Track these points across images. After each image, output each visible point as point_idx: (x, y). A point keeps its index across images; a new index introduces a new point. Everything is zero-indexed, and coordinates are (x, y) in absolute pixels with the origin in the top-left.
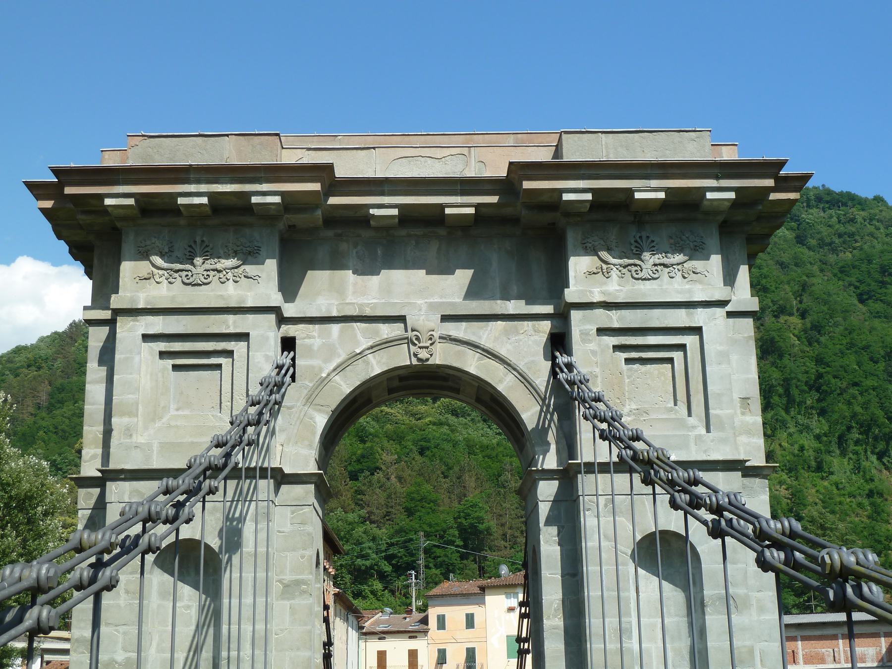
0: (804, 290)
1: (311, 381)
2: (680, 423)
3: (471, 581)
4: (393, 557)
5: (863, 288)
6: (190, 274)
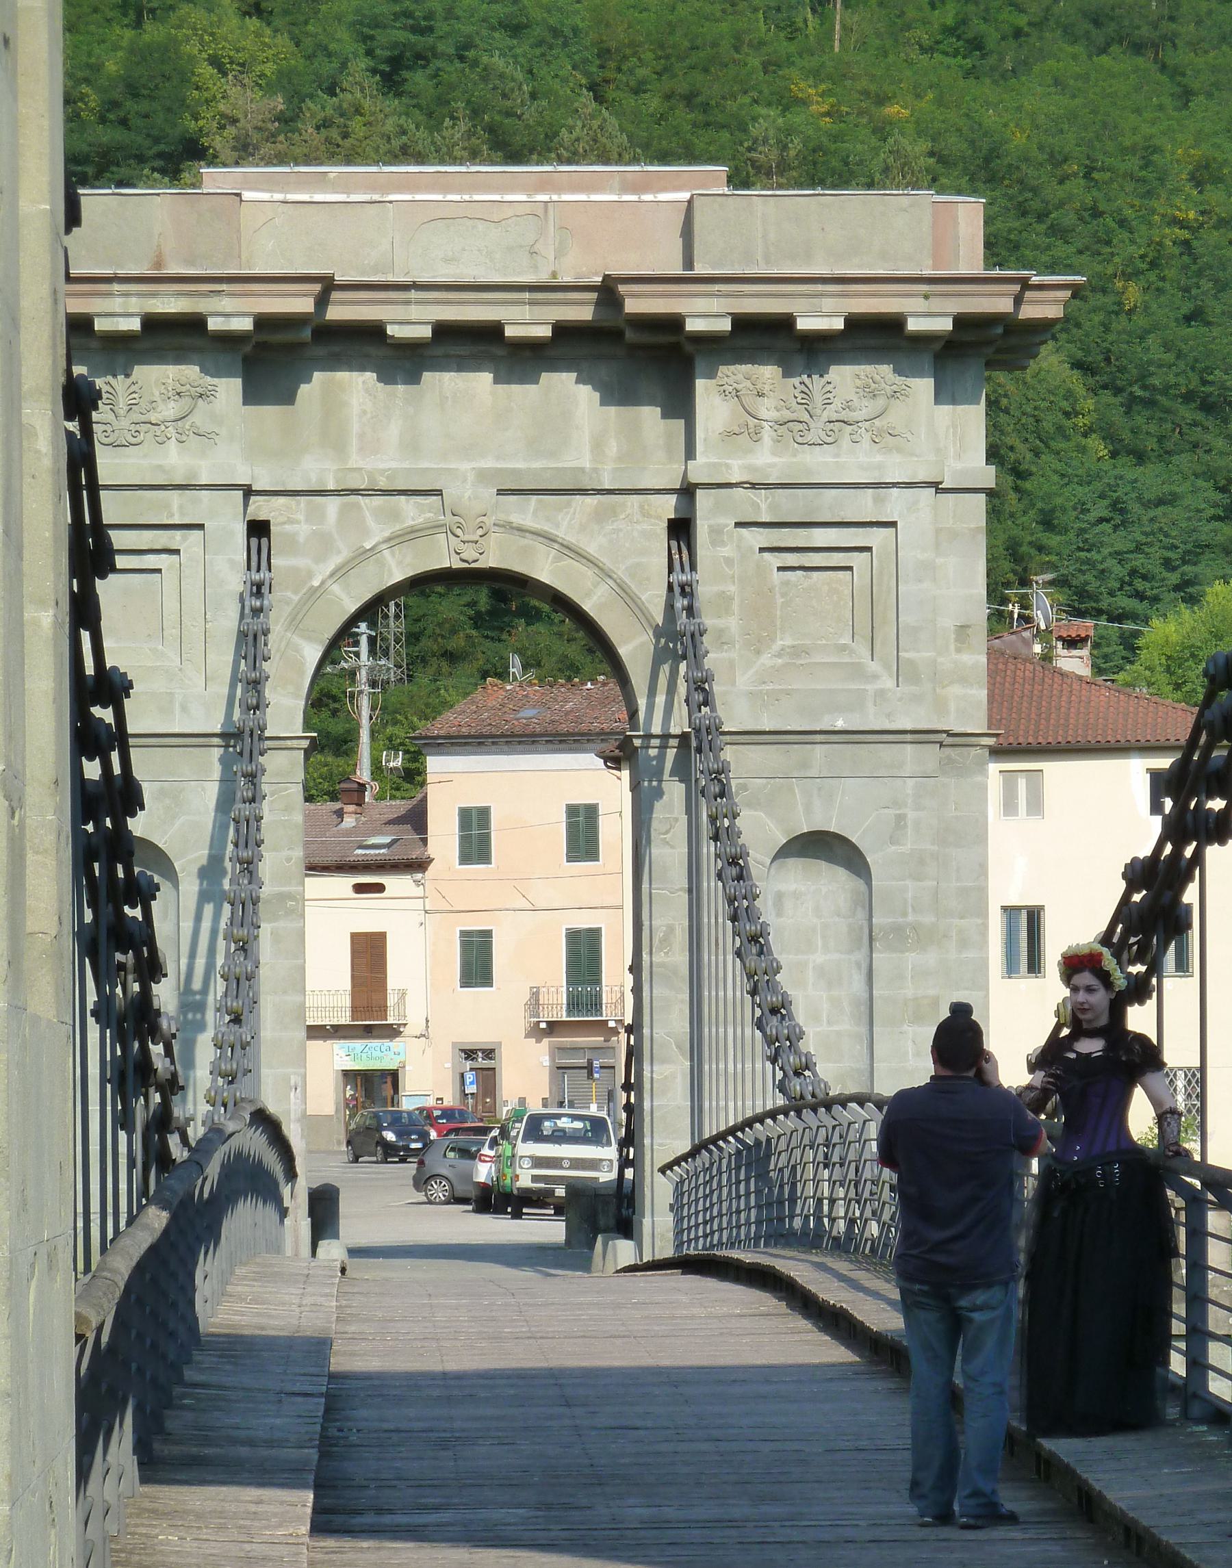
1: (295, 592)
2: (857, 671)
3: (589, 685)
6: (108, 428)
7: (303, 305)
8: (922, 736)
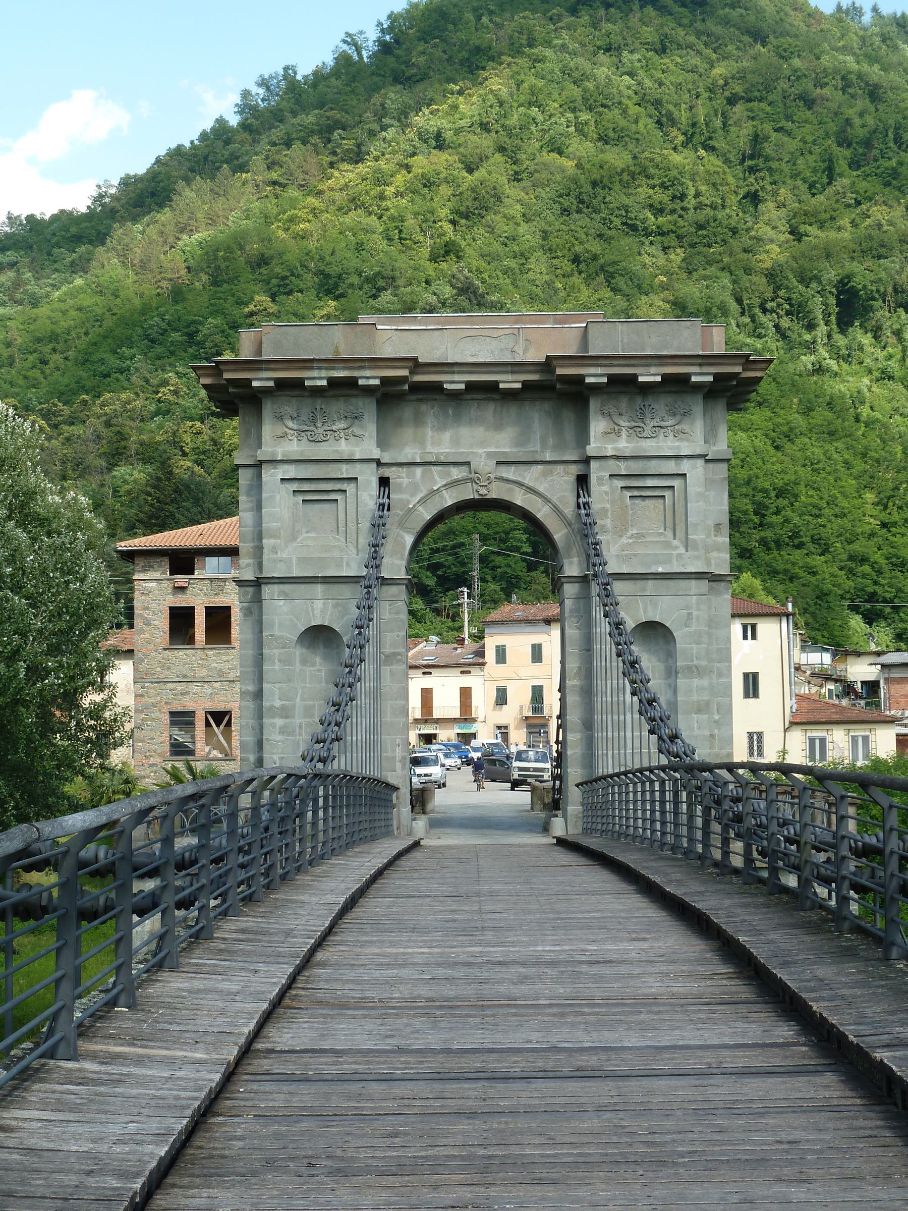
2: (668, 545)
4: (438, 566)
7: (404, 373)
8: (699, 576)
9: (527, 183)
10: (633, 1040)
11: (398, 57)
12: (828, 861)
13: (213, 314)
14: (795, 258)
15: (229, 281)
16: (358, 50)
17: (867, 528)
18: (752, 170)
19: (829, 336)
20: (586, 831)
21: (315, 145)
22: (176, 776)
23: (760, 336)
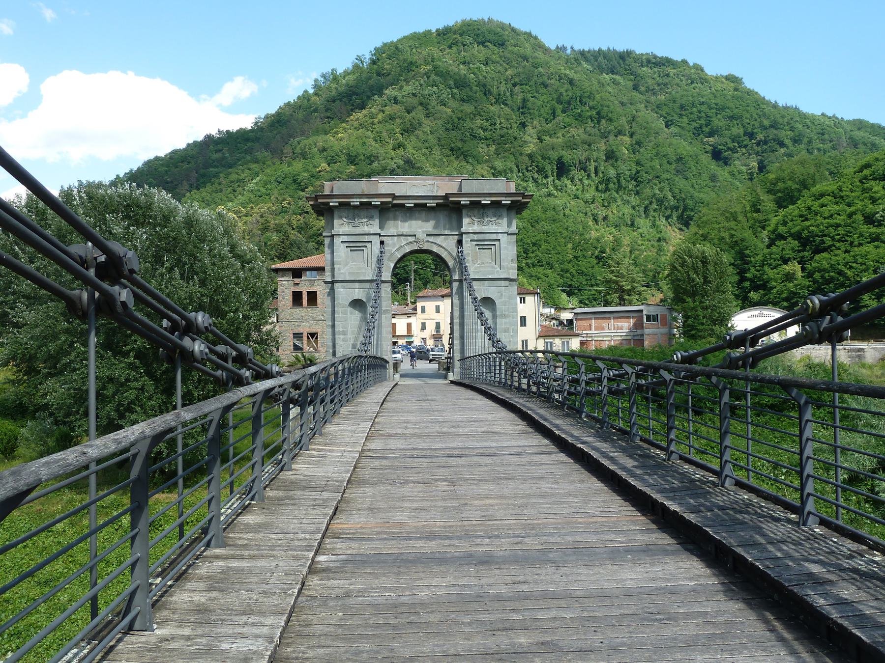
0: (633, 120)
2: (493, 267)
5: (669, 118)
7: (390, 200)
9: (431, 118)
10: (494, 445)
11: (378, 66)
12: (559, 384)
13: (304, 171)
14: (540, 150)
15: (311, 158)
16: (362, 62)
17: (568, 259)
18: (523, 113)
19: (554, 181)
20: (461, 378)
21: (345, 102)
22: (297, 358)
23: (526, 181)
